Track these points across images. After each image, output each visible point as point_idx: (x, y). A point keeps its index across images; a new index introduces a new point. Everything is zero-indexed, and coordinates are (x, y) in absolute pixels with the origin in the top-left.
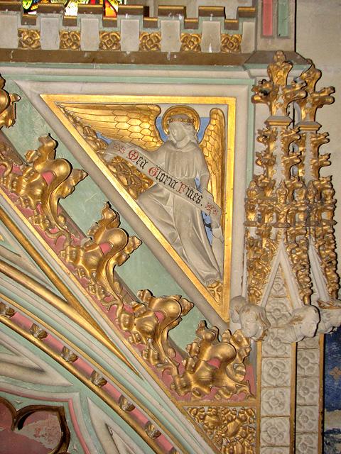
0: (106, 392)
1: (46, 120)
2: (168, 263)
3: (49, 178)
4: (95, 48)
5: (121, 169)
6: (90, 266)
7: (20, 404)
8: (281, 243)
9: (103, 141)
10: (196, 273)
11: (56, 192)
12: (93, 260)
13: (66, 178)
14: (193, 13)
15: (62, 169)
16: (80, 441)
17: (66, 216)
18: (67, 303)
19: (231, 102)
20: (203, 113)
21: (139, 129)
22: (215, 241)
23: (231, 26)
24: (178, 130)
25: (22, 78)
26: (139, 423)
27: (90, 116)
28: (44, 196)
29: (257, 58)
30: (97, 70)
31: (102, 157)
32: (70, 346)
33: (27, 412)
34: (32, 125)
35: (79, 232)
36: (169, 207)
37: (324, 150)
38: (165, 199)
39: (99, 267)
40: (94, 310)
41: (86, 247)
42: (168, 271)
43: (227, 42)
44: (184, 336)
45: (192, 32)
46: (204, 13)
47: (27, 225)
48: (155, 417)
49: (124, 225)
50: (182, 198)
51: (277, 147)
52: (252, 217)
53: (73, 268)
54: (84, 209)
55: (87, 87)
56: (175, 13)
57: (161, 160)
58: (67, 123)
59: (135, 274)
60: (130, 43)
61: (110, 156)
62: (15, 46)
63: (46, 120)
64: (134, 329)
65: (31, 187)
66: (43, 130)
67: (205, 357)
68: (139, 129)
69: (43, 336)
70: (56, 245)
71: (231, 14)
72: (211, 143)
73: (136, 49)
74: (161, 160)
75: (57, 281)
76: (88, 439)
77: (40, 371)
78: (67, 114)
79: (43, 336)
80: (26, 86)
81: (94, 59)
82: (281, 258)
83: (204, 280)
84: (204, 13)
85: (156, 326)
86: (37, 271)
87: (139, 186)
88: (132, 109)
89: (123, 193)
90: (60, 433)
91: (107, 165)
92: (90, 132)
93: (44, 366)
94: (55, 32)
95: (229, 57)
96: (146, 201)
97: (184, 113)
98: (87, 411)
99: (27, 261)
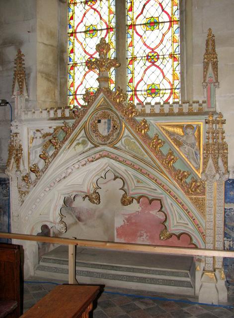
0: (171, 194)
1: (157, 130)
2: (186, 164)
3: (157, 143)
4: (168, 112)
5: (175, 141)
6: (166, 163)
7: (151, 198)
8: (210, 158)
9: (171, 134)
10: (193, 166)
11: (158, 146)
12: (167, 162)
13: (161, 143)
14: (191, 102)
15: (160, 141)
16: (165, 207)
17: (161, 152)
18: (161, 172)
19: (202, 123)
20: (195, 126)
21: (179, 131)
22: (198, 158)
23: (200, 105)
24: (189, 131)
25: (151, 119)
26: (159, 184)
27: (167, 128)
28: (156, 147)
29: (206, 113)
30: (168, 117)
31: (170, 137)
32: (163, 184)
33: (153, 200)
34: (153, 131)
35: (164, 155)
36: (186, 150)
37: (224, 135)
38: (185, 148)
39: (168, 163)
40: (167, 174)
41: (165, 159)
42: (185, 165)
43: (200, 110)
44: (188, 180)
45: (191, 107)
46: (194, 102)
47: (152, 154)
48: (132, 162)
49: (175, 154)
50: (190, 147)
51: (210, 135)
52: (205, 152)
53: (162, 164)
54: (165, 150)
55: (166, 121)
56: (187, 103)
57: (184, 138)
58: (161, 129)
59: (177, 166)
60: (185, 110)
61: (172, 138)
62: (149, 112)
63: (157, 130)
64: (176, 178)
65: (153, 145)
66: (156, 131)
67: (193, 185)
68: (179, 131)
69: (149, 175)
70: (159, 159)
71: (162, 103)
72: (196, 133)
73: (177, 112)
74: (184, 138)
75: (159, 167)
76: (167, 207)
77: (156, 190)
78: (162, 128)
79: (183, 205)
80: (152, 121)
81: (167, 115)
82: (210, 162)
83: (195, 168)
84: (194, 102)
85: (181, 178)
86: (155, 165)
87: (179, 144)
88: (177, 126)
89: (175, 146)
90: (160, 206)
91: (172, 139)
92: (167, 132)
93: (156, 188)
94: (158, 108)
95: (200, 113)
96: (181, 148)
97: (189, 126)
98: (166, 200)
99: (152, 162)
